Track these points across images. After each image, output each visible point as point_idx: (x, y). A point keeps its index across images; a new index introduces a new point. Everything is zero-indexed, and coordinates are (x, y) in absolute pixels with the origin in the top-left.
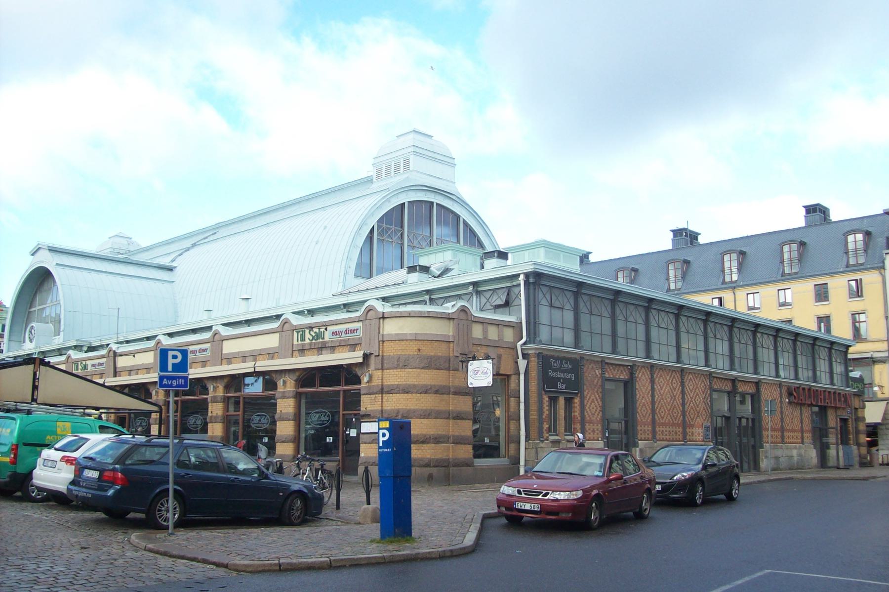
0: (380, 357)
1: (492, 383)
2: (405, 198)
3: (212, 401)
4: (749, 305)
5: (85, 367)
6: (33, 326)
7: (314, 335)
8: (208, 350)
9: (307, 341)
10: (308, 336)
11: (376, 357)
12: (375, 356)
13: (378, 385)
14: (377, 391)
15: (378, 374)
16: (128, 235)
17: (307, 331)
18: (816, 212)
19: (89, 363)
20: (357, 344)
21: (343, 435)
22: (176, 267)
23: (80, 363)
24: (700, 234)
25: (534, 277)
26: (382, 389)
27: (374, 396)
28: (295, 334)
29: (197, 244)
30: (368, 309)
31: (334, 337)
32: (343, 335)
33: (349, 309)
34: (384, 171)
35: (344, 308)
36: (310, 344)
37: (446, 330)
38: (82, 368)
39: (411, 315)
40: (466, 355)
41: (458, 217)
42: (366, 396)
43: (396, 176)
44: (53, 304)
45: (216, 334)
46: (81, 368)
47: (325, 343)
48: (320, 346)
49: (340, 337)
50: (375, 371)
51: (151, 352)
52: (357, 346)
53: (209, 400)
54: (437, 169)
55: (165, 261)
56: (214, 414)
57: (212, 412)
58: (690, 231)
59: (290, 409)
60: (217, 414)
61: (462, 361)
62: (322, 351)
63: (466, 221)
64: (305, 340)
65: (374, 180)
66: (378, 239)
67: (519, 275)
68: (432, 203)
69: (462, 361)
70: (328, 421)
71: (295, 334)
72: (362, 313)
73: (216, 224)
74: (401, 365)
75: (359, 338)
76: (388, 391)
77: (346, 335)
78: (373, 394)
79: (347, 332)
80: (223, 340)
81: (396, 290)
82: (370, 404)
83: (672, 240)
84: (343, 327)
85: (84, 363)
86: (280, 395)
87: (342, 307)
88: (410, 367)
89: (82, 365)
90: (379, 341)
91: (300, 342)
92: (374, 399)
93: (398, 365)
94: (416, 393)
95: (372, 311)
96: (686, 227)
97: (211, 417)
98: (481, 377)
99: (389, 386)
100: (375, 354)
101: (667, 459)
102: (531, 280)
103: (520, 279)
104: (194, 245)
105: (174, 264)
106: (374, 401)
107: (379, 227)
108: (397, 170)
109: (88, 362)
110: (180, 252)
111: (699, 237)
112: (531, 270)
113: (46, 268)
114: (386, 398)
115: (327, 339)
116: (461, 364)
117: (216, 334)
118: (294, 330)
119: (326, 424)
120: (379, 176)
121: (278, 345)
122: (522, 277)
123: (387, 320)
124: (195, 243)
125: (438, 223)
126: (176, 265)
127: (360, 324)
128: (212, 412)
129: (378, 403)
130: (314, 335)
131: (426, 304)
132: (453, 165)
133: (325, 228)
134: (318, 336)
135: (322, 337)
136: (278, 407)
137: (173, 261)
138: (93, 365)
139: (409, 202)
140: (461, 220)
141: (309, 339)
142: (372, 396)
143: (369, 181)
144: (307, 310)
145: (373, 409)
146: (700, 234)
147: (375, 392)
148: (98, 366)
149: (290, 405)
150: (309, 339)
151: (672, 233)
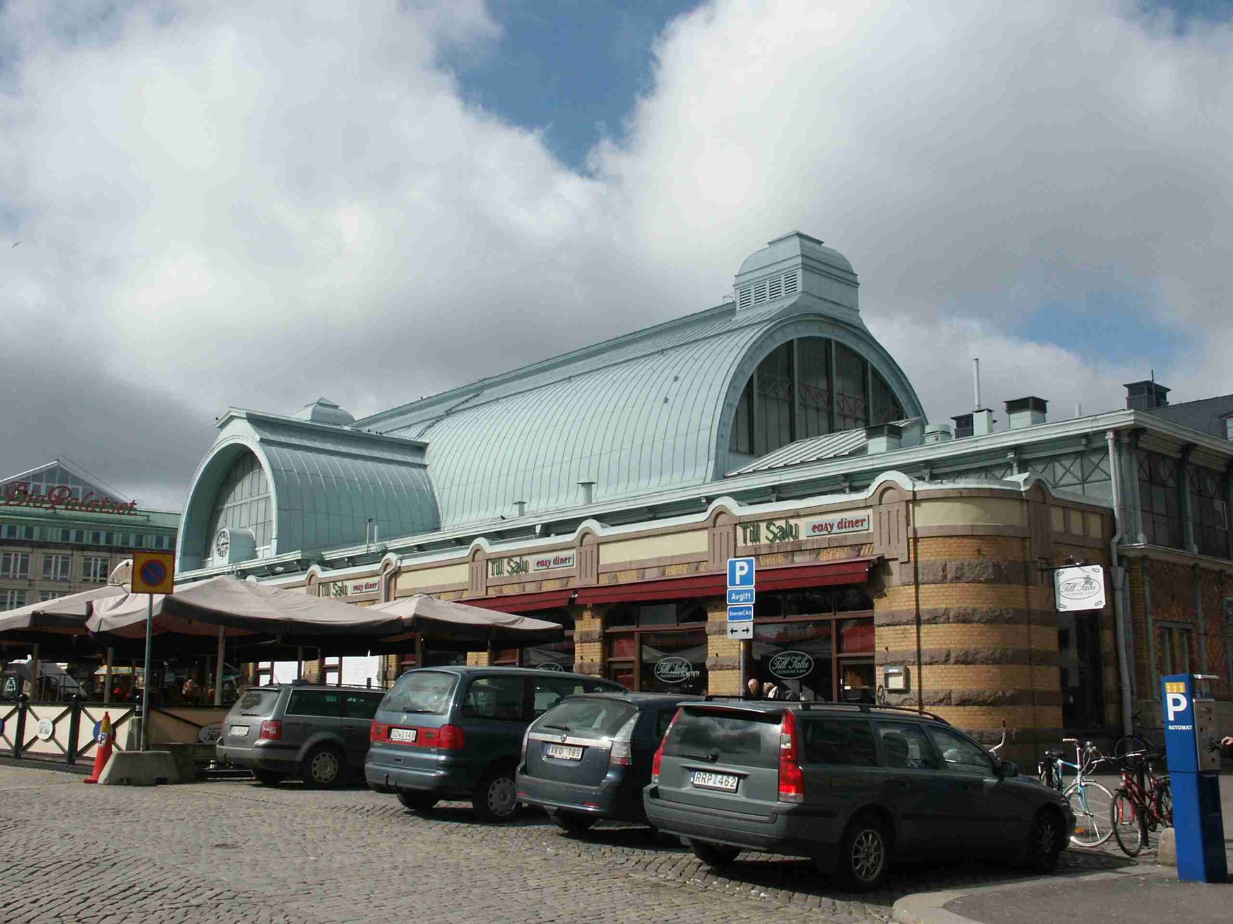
0: (912, 564)
1: (1104, 604)
2: (792, 334)
3: (581, 639)
4: (890, 563)
5: (521, 567)
6: (224, 532)
7: (776, 531)
8: (571, 560)
9: (764, 541)
10: (506, 568)
11: (903, 565)
12: (901, 563)
13: (908, 611)
14: (908, 621)
15: (909, 591)
16: (336, 403)
17: (763, 526)
18: (134, 503)
19: (350, 584)
20: (862, 545)
21: (839, 693)
22: (427, 445)
23: (332, 584)
24: (1169, 390)
25: (1129, 435)
26: (918, 616)
27: (902, 627)
28: (740, 530)
29: (454, 410)
30: (882, 488)
31: (540, 568)
32: (835, 530)
33: (781, 495)
34: (753, 295)
35: (773, 493)
36: (770, 547)
37: (1013, 516)
38: (337, 591)
39: (964, 495)
40: (1046, 559)
41: (864, 362)
42: (886, 628)
43: (757, 306)
44: (253, 499)
45: (478, 550)
46: (335, 592)
47: (801, 543)
48: (789, 549)
49: (830, 534)
50: (902, 588)
51: (700, 533)
52: (864, 547)
53: (576, 638)
54: (835, 291)
55: (410, 435)
56: (587, 661)
57: (582, 658)
58: (1157, 386)
59: (734, 650)
60: (592, 660)
61: (1042, 570)
62: (793, 557)
63: (876, 370)
64: (759, 540)
65: (738, 308)
66: (759, 395)
67: (1104, 432)
68: (828, 341)
69: (1042, 570)
70: (808, 669)
71: (740, 530)
72: (870, 494)
73: (479, 382)
74: (949, 576)
75: (868, 534)
76: (928, 620)
77: (841, 531)
78: (899, 625)
79: (841, 524)
80: (598, 544)
81: (783, 477)
82: (893, 640)
83: (1128, 399)
84: (363, 582)
85: (339, 584)
86: (715, 629)
87: (771, 490)
88: (965, 579)
89: (336, 587)
90: (908, 539)
91: (749, 544)
92: (903, 633)
93: (945, 577)
94: (978, 622)
95: (724, 515)
96: (1150, 379)
97: (581, 666)
98: (1081, 594)
99: (929, 612)
100: (901, 560)
101: (1112, 797)
102: (1126, 440)
103: (1106, 437)
104: (449, 413)
105: (423, 440)
106: (902, 636)
107: (759, 376)
108: (775, 291)
109: (346, 583)
110: (429, 423)
111: (1168, 394)
112: (1128, 423)
113: (246, 446)
114: (925, 631)
115: (802, 537)
116: (1040, 573)
117: (478, 550)
118: (736, 525)
119: (803, 673)
120: (745, 302)
121: (707, 550)
122: (1110, 435)
123: (924, 505)
124: (450, 410)
125: (838, 374)
126: (427, 441)
127: (870, 511)
128: (582, 658)
129: (911, 639)
130: (514, 565)
131: (844, 492)
132: (855, 285)
133: (676, 379)
134: (786, 532)
135: (794, 534)
136: (709, 648)
137: (421, 435)
138: (356, 588)
139: (799, 339)
140: (869, 365)
141: (508, 571)
142: (898, 627)
143: (726, 311)
144: (706, 497)
145: (899, 649)
146: (1169, 390)
147: (905, 620)
148: (366, 588)
149: (734, 645)
150: (508, 571)
151: (1127, 389)
